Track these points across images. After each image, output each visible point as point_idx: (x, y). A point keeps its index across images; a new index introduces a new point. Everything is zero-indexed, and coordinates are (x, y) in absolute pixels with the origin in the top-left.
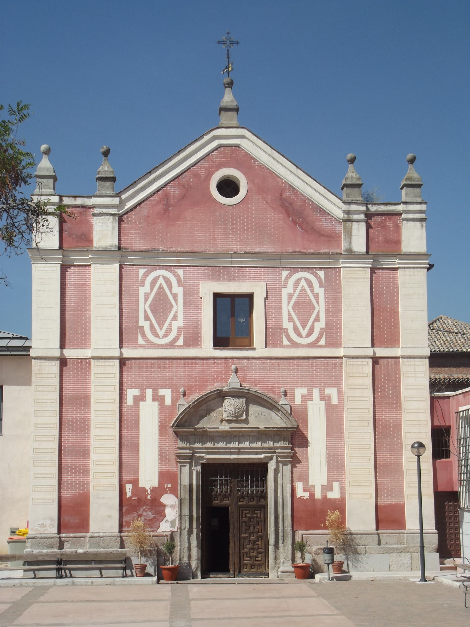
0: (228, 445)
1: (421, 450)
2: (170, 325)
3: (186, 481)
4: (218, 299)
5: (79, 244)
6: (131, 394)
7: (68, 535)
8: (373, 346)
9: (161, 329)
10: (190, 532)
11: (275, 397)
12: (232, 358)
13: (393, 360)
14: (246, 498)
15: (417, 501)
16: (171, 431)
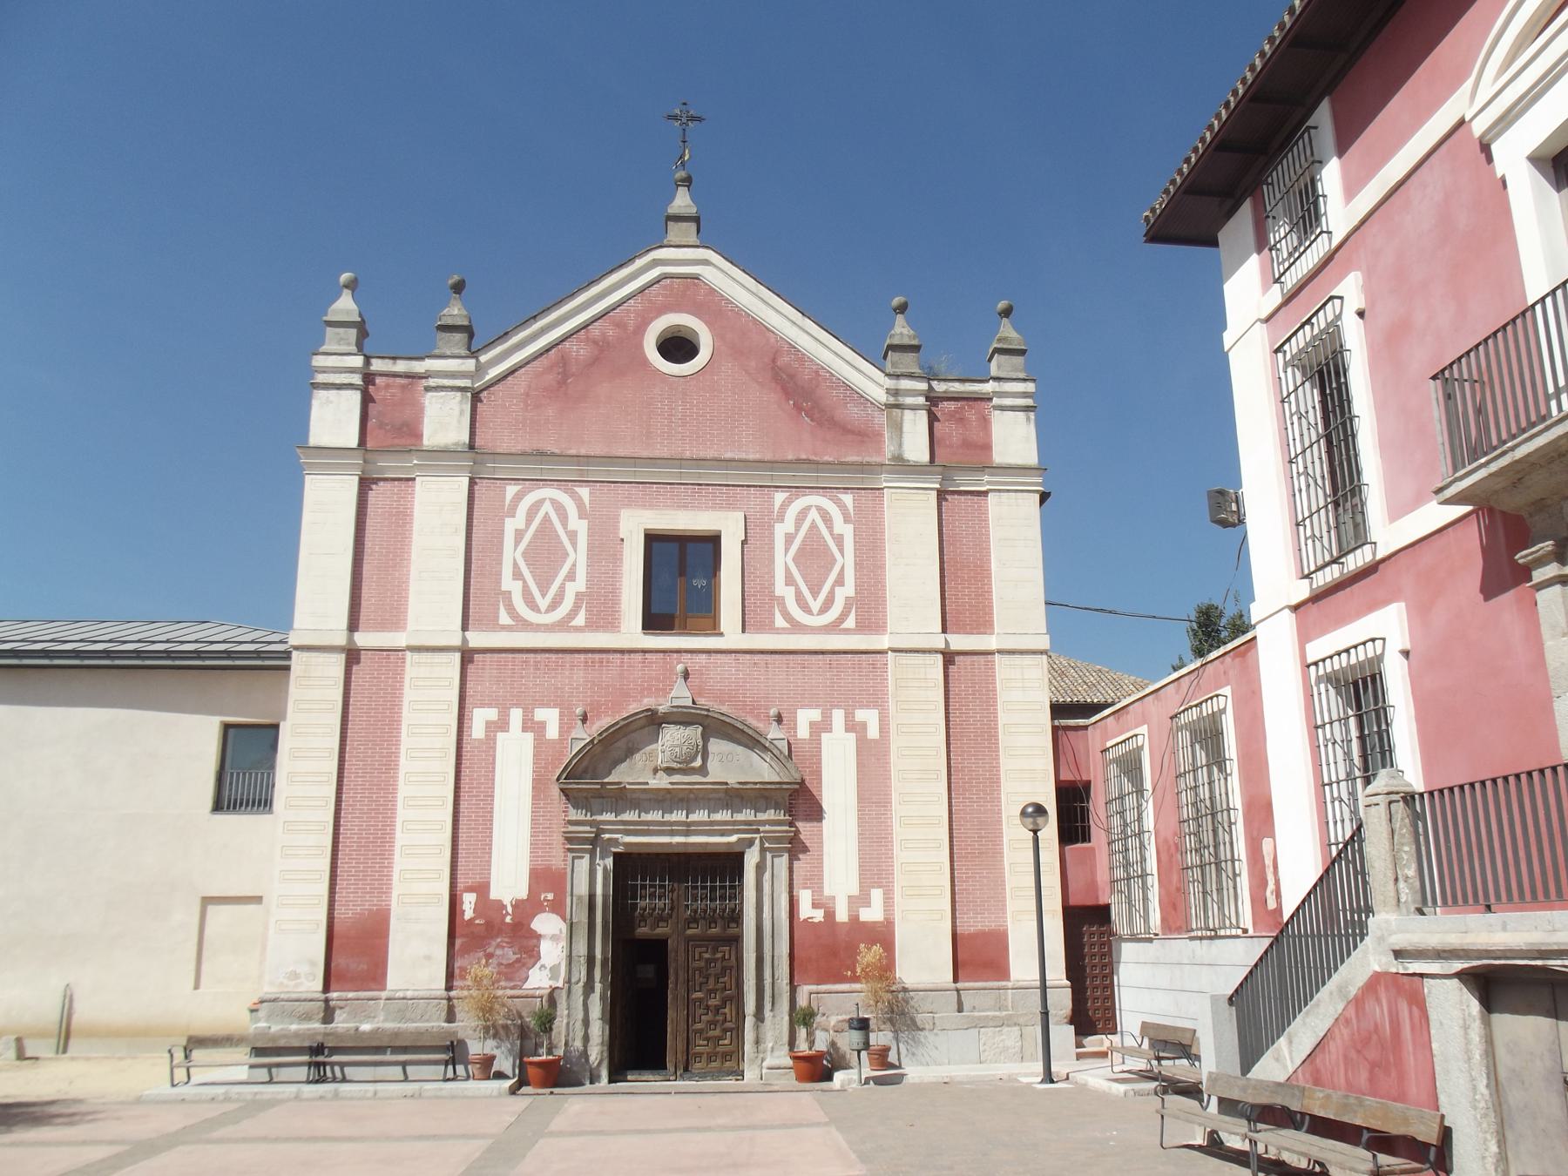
0: (668, 817)
1: (1040, 820)
2: (562, 589)
3: (582, 888)
4: (655, 545)
5: (396, 441)
6: (481, 718)
7: (344, 995)
8: (944, 631)
9: (544, 596)
10: (589, 988)
11: (760, 726)
12: (678, 651)
13: (982, 658)
14: (701, 922)
15: (1035, 924)
16: (555, 790)
